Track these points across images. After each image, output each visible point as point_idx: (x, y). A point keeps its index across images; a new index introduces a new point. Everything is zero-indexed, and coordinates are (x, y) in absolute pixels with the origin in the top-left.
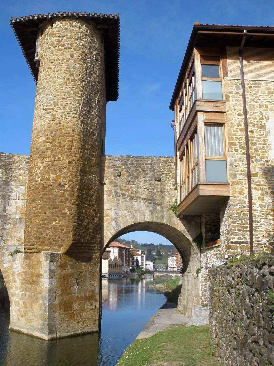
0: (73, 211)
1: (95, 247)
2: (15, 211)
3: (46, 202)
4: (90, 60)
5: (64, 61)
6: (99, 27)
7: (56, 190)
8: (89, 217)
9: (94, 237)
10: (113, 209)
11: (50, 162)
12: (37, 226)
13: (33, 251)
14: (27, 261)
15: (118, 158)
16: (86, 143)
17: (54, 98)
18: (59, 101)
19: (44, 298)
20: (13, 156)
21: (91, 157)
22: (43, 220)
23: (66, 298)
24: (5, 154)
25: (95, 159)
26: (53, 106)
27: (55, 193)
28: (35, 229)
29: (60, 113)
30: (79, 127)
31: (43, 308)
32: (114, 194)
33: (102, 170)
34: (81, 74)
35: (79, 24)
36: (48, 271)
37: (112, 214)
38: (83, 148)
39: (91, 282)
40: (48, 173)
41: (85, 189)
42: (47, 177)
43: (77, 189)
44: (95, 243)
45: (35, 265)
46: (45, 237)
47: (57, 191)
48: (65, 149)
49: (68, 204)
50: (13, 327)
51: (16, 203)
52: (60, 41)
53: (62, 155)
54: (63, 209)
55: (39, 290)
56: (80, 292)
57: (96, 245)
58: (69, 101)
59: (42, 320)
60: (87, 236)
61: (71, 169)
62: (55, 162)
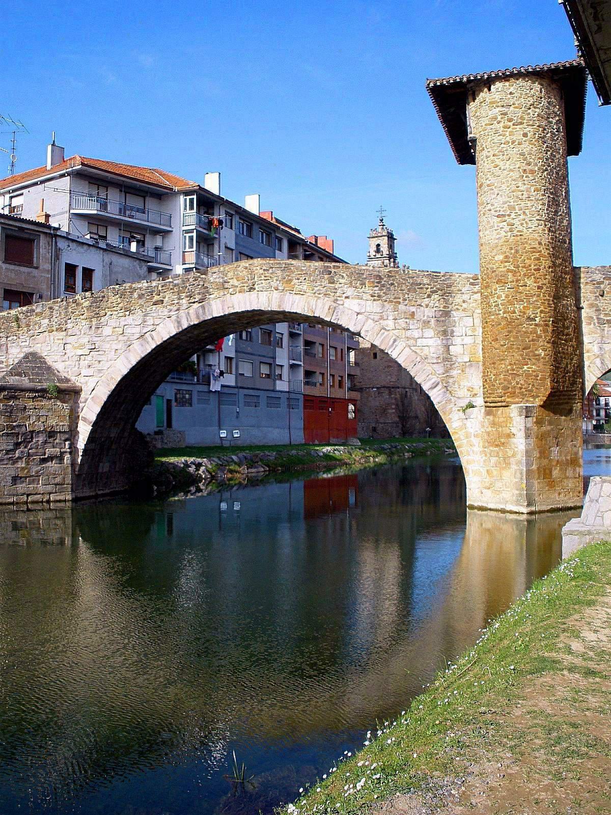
0: (549, 351)
1: (576, 395)
2: (462, 352)
3: (513, 342)
4: (549, 135)
5: (515, 143)
6: (556, 78)
7: (525, 325)
8: (567, 357)
9: (574, 383)
10: (596, 342)
11: (513, 288)
12: (504, 373)
13: (499, 404)
14: (491, 418)
15: (599, 270)
16: (557, 258)
17: (509, 199)
18: (516, 204)
19: (519, 463)
20: (451, 276)
21: (563, 275)
22: (511, 364)
23: (545, 462)
24: (440, 273)
25: (568, 277)
26: (509, 211)
27: (524, 329)
28: (502, 376)
29: (519, 221)
30: (546, 238)
31: (518, 475)
32: (596, 321)
33: (577, 289)
34: (541, 161)
35: (529, 83)
36: (523, 429)
37: (595, 349)
38: (554, 265)
39: (572, 441)
40: (512, 304)
41: (561, 320)
42: (512, 309)
43: (551, 322)
44: (575, 391)
45: (504, 421)
46: (515, 387)
47: (527, 327)
48: (531, 270)
49: (541, 342)
50: (472, 503)
51: (463, 340)
52: (506, 114)
53: (528, 278)
54: (536, 350)
55: (510, 453)
56: (561, 456)
57: (577, 392)
58: (529, 202)
59: (517, 490)
60: (566, 381)
61: (541, 296)
62: (520, 288)
